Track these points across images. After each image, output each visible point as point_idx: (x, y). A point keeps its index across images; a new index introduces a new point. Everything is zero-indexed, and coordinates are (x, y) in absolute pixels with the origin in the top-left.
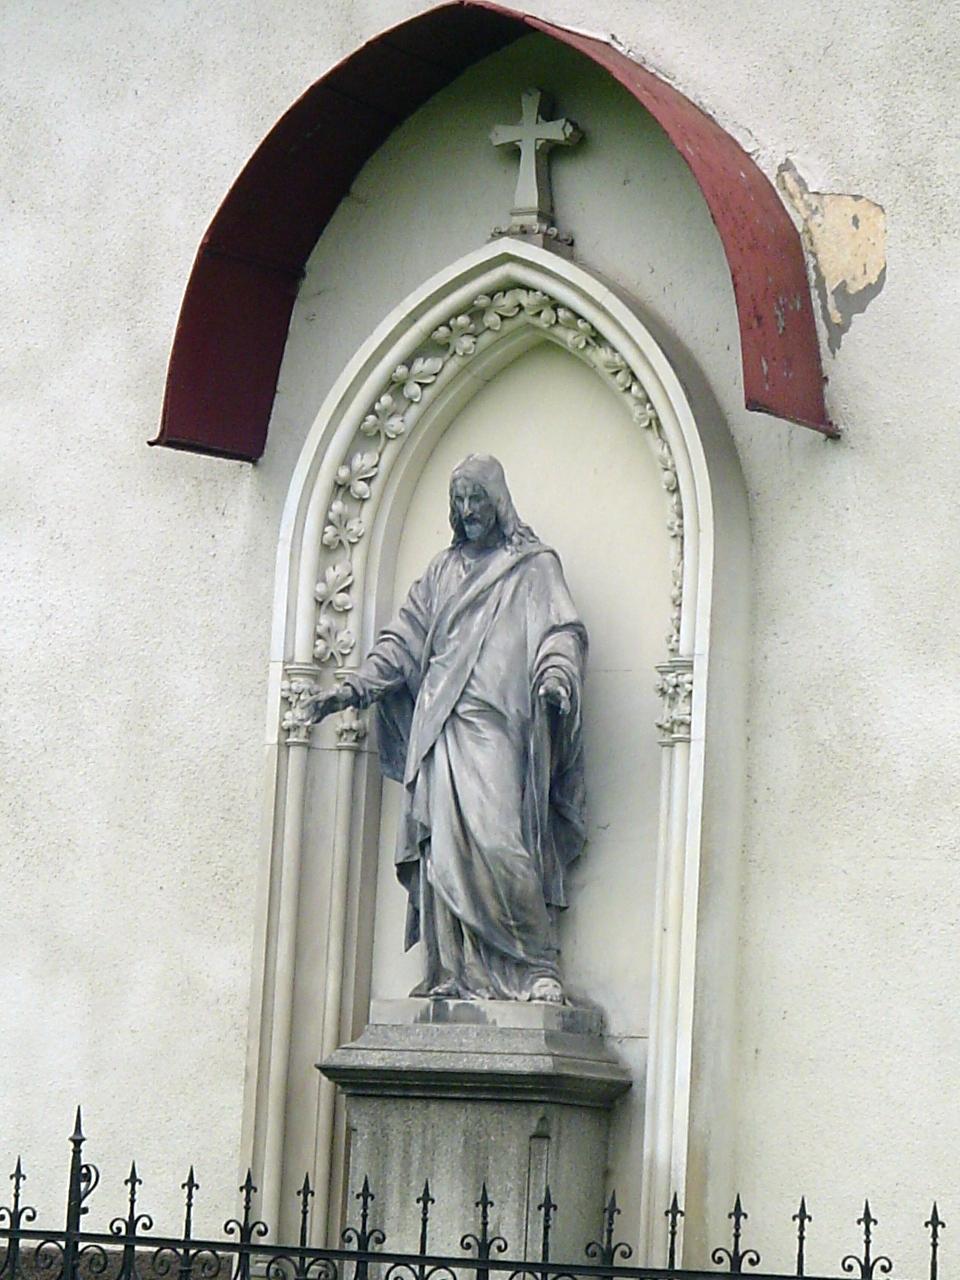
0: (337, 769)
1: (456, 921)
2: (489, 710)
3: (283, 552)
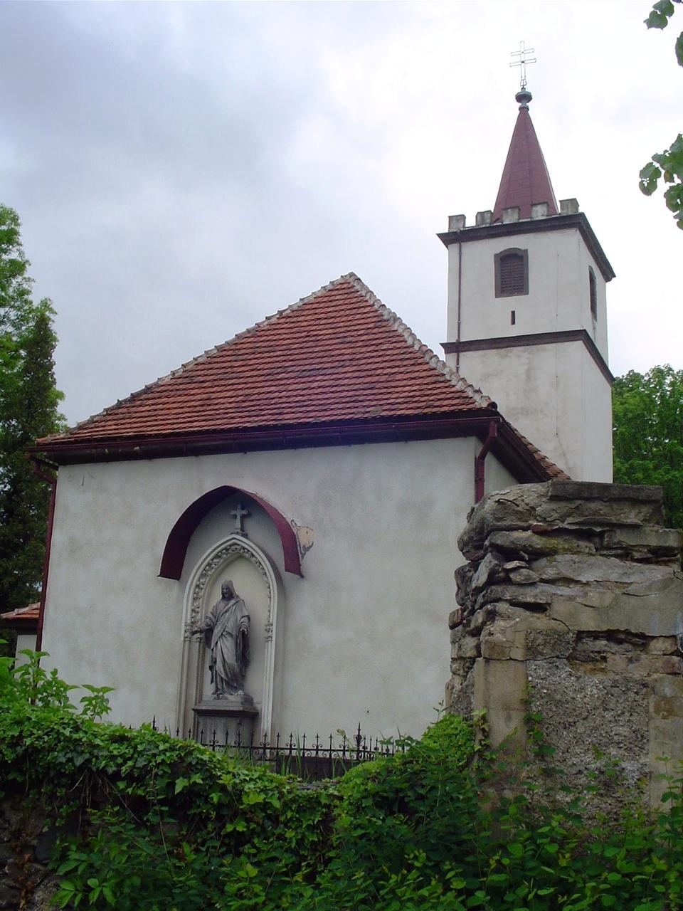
2: (229, 634)
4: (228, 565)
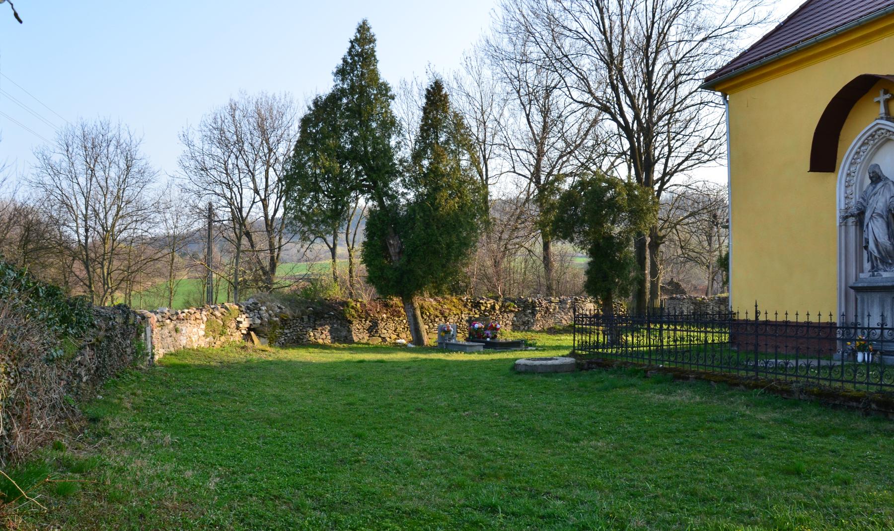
0: (852, 230)
1: (876, 257)
2: (879, 215)
3: (838, 186)
4: (879, 148)
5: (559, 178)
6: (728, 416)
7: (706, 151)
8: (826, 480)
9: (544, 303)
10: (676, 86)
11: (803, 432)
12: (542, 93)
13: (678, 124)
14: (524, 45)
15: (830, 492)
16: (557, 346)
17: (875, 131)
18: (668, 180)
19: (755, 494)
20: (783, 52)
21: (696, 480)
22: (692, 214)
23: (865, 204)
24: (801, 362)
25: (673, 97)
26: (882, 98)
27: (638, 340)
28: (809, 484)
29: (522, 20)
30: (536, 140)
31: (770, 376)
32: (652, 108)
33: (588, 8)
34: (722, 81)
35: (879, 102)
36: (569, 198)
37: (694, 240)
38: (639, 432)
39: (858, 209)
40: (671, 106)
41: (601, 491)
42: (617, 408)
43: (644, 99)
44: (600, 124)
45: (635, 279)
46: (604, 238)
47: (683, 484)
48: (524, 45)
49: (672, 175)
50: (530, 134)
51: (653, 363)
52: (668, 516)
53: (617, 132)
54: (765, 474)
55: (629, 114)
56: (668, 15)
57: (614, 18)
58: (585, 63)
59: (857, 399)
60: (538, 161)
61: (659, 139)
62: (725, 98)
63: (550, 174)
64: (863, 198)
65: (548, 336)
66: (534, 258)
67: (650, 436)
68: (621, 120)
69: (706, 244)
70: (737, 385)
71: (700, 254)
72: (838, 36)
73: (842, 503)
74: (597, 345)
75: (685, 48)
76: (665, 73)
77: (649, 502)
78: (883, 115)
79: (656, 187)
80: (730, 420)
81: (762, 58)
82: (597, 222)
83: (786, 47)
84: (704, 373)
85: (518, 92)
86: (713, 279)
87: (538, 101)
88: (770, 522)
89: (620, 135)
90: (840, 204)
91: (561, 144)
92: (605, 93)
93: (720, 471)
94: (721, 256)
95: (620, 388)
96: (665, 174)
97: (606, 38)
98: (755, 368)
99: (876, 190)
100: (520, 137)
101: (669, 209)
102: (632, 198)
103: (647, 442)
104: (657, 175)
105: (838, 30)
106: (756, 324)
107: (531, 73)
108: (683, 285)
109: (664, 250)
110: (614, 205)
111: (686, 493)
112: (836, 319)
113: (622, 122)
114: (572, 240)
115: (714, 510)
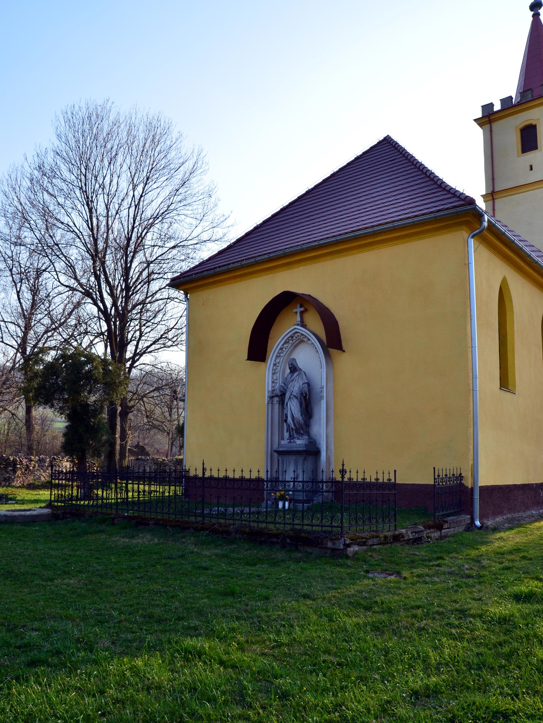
0: (276, 407)
1: (292, 428)
2: (295, 396)
3: (267, 372)
4: (296, 346)
5: (44, 351)
6: (180, 553)
7: (170, 337)
8: (253, 598)
9: (24, 461)
10: (149, 282)
11: (237, 563)
12: (33, 274)
13: (149, 314)
14: (20, 229)
15: (256, 606)
16: (35, 500)
17: (294, 334)
18: (138, 360)
19: (200, 613)
20: (231, 266)
21: (153, 605)
22: (157, 389)
23: (285, 388)
24: (237, 510)
25: (146, 291)
26: (299, 310)
27: (107, 495)
28: (240, 602)
29: (20, 207)
30: (24, 315)
31: (214, 521)
32: (127, 298)
33: (79, 206)
34: (186, 283)
35: (296, 312)
36: (51, 367)
37: (158, 411)
38: (107, 570)
39: (281, 391)
40: (144, 297)
41: (73, 620)
42: (88, 550)
43: (122, 290)
44: (83, 306)
45: (107, 441)
46: (81, 405)
47: (142, 609)
48: (20, 229)
49: (141, 355)
50: (20, 310)
51: (120, 512)
52: (130, 636)
53: (97, 315)
54: (208, 597)
55: (109, 301)
56: (146, 223)
57: (101, 218)
58: (74, 253)
59: (276, 536)
60: (26, 333)
61: (132, 324)
62: (186, 296)
63: (35, 346)
64: (284, 383)
65: (27, 491)
66: (17, 421)
67: (116, 573)
68: (101, 305)
69: (167, 414)
70: (188, 528)
71: (163, 422)
72: (270, 260)
73: (263, 614)
74: (71, 498)
75: (158, 252)
76: (141, 270)
77: (114, 627)
78: (299, 323)
79: (128, 365)
80: (182, 556)
81: (216, 268)
82: (75, 391)
83: (234, 263)
84: (161, 520)
85: (11, 270)
86: (172, 444)
87: (28, 281)
88: (211, 633)
89: (99, 318)
90: (268, 387)
91: (47, 321)
92: (89, 280)
93: (172, 597)
94: (178, 425)
95: (91, 534)
96: (135, 354)
97: (93, 234)
98: (203, 515)
99: (293, 378)
100: (9, 311)
101: (138, 383)
102: (107, 372)
103: (113, 577)
104: (128, 355)
105: (271, 255)
106: (203, 479)
107: (24, 256)
108: (148, 449)
109: (132, 418)
110: (91, 377)
111: (145, 617)
112: (263, 476)
113: (102, 307)
114: (52, 406)
115: (167, 628)
